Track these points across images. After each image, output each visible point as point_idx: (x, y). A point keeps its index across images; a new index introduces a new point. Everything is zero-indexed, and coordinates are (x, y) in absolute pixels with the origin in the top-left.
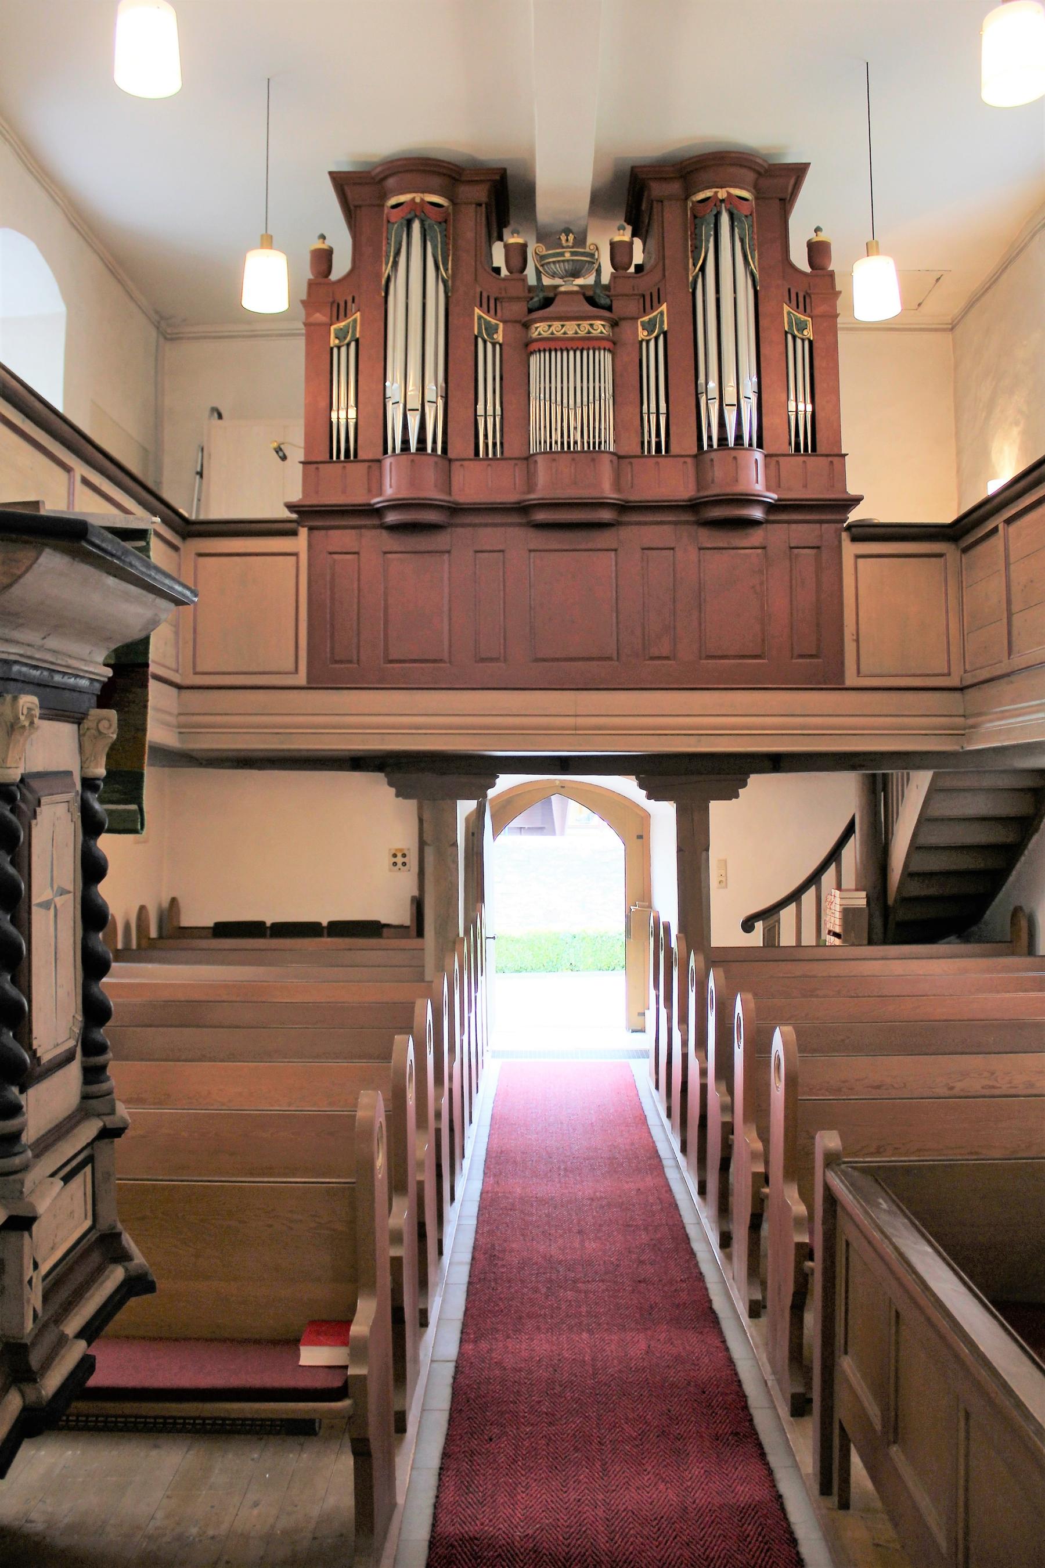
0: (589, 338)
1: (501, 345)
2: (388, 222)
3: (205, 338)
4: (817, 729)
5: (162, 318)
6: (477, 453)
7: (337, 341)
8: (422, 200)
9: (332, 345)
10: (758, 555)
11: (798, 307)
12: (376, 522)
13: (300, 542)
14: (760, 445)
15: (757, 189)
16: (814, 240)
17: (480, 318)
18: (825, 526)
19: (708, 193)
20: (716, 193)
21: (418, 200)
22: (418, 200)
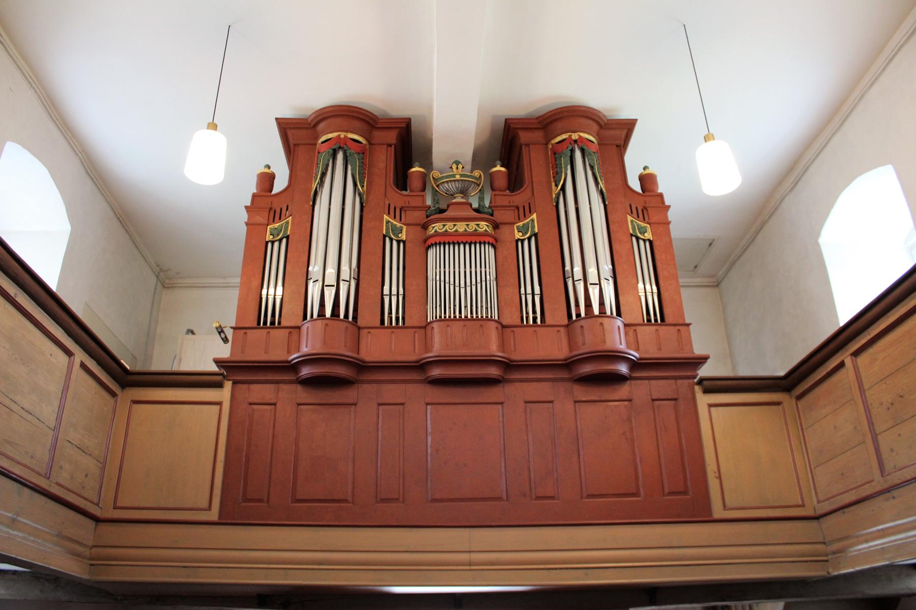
0: (475, 233)
1: (404, 242)
2: (319, 153)
3: (191, 287)
4: (702, 559)
5: (161, 270)
6: (382, 321)
7: (271, 237)
8: (345, 137)
9: (267, 240)
10: (625, 406)
11: (638, 217)
12: (292, 377)
13: (224, 394)
14: (619, 314)
15: (598, 136)
16: (643, 174)
17: (388, 222)
18: (680, 382)
19: (564, 136)
20: (570, 136)
21: (342, 136)
22: (342, 136)
